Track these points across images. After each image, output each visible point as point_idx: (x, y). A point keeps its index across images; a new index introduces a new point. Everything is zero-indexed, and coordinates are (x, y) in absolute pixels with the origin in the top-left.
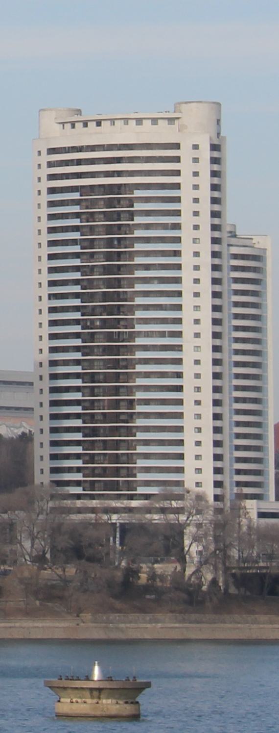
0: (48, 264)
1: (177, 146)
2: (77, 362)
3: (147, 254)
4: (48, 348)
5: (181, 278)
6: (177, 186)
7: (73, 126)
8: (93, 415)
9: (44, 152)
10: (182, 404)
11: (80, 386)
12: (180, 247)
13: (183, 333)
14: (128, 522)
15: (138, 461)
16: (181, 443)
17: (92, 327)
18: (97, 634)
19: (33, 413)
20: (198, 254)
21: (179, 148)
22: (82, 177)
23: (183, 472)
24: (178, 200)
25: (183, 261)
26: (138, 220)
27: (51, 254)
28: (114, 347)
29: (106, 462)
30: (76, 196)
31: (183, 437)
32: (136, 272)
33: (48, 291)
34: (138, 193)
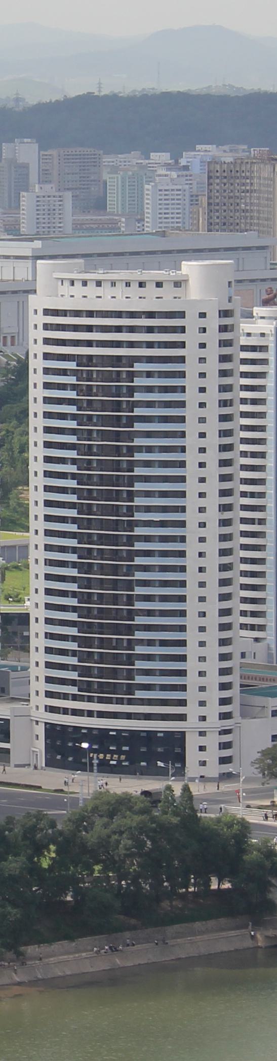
0: (44, 438)
1: (182, 315)
2: (73, 432)
3: (148, 435)
4: (42, 457)
5: (185, 596)
6: (182, 359)
7: (72, 283)
8: (89, 462)
9: (40, 312)
10: (185, 601)
11: (76, 577)
12: (186, 695)
13: (183, 349)
14: (119, 156)
15: (136, 647)
16: (183, 643)
17: (89, 482)
18: (87, 234)
19: (28, 490)
20: (204, 419)
21: (184, 526)
22: (79, 345)
23: (186, 675)
24: (182, 375)
25: (188, 562)
26: (138, 501)
27: (48, 589)
28: (112, 536)
29: (99, 394)
30: (72, 365)
31: (186, 577)
32: (136, 528)
33: (43, 379)
34: (138, 367)
